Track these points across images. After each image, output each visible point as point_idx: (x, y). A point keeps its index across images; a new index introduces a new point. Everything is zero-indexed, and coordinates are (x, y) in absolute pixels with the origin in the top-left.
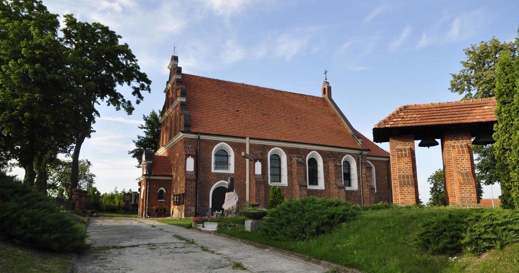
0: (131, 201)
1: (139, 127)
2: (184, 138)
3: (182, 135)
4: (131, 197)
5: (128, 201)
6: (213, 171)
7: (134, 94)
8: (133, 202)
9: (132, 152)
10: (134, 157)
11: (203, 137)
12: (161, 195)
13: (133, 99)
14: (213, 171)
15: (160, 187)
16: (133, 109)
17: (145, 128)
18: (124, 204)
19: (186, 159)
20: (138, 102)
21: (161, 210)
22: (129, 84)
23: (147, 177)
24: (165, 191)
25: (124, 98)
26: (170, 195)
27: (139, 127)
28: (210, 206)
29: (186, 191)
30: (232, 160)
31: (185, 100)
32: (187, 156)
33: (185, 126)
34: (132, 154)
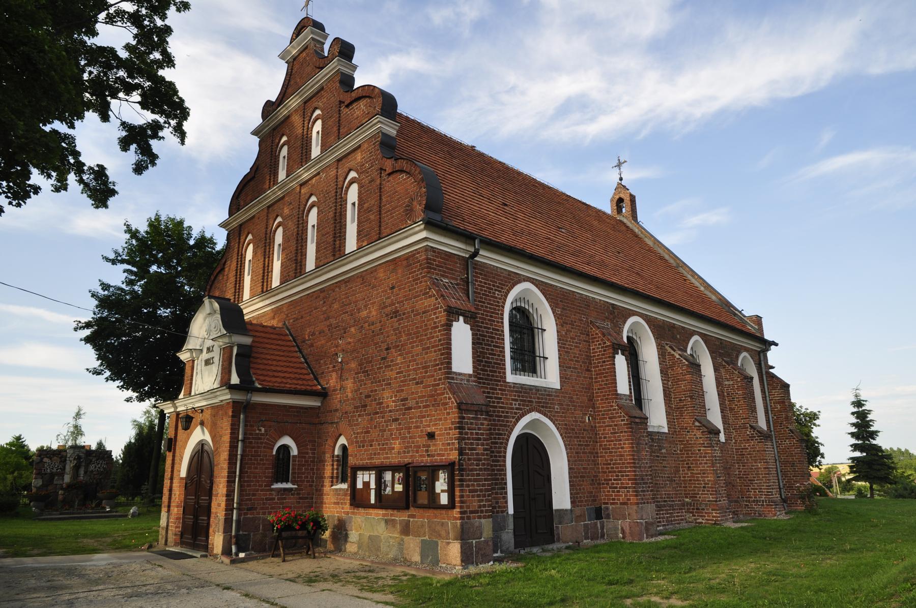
0: (62, 475)
1: (107, 259)
2: (427, 249)
3: (424, 234)
4: (63, 460)
5: (52, 475)
6: (511, 378)
7: (125, 144)
8: (67, 479)
9: (88, 325)
10: (87, 340)
11: (487, 257)
12: (282, 465)
13: (119, 164)
14: (511, 378)
15: (280, 437)
16: (113, 193)
17: (123, 261)
18: (40, 482)
19: (448, 326)
20: (139, 169)
21: (303, 526)
22: (105, 118)
23: (239, 397)
24: (294, 451)
25: (82, 159)
26: (322, 461)
27: (107, 259)
28: (511, 511)
29: (461, 452)
30: (549, 343)
31: (393, 132)
32: (453, 314)
33: (428, 207)
34: (87, 332)
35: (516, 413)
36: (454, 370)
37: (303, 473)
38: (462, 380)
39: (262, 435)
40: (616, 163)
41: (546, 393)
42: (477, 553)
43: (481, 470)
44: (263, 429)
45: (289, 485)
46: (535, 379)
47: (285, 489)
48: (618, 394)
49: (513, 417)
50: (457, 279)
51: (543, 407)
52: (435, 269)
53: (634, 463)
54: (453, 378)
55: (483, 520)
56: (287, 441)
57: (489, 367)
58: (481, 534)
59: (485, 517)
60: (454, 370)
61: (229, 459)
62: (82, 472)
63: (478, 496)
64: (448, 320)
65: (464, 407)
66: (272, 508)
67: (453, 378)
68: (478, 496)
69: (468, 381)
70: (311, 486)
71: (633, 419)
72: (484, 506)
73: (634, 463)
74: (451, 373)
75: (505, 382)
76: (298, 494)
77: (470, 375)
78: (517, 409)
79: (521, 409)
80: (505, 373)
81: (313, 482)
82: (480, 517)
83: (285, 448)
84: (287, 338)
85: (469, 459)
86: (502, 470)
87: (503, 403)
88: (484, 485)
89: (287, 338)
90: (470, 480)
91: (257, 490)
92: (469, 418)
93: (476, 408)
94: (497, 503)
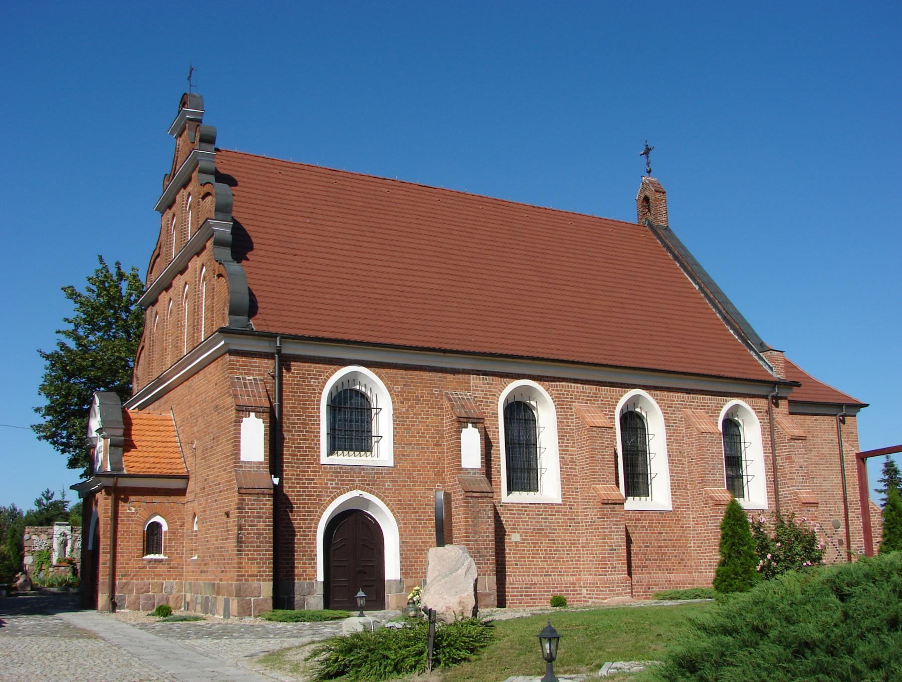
14: (324, 459)
19: (238, 422)
24: (165, 528)
28: (320, 577)
30: (383, 424)
35: (332, 492)
36: (242, 459)
37: (173, 546)
38: (251, 467)
39: (133, 513)
40: (651, 154)
41: (378, 471)
42: (255, 607)
43: (261, 542)
44: (133, 509)
45: (161, 557)
46: (369, 458)
47: (156, 560)
48: (462, 469)
49: (328, 496)
50: (263, 375)
51: (369, 485)
52: (239, 369)
53: (467, 537)
54: (241, 467)
55: (262, 583)
56: (158, 519)
57: (299, 451)
58: (260, 593)
59: (264, 580)
60: (242, 459)
61: (496, 531)
62: (68, 549)
63: (258, 563)
64: (237, 417)
65: (243, 491)
66: (145, 575)
67: (241, 467)
68: (258, 563)
69: (258, 468)
70: (181, 557)
71: (469, 494)
72: (264, 571)
73: (467, 537)
74: (239, 462)
75: (319, 464)
76: (169, 564)
77: (261, 463)
78: (333, 488)
79: (339, 488)
80: (319, 456)
81: (183, 554)
82: (259, 580)
83: (157, 525)
84: (170, 423)
85: (249, 534)
86: (312, 543)
87: (315, 483)
88: (265, 555)
89: (170, 423)
90: (249, 551)
91: (130, 560)
92: (250, 500)
93: (257, 491)
94: (305, 571)
